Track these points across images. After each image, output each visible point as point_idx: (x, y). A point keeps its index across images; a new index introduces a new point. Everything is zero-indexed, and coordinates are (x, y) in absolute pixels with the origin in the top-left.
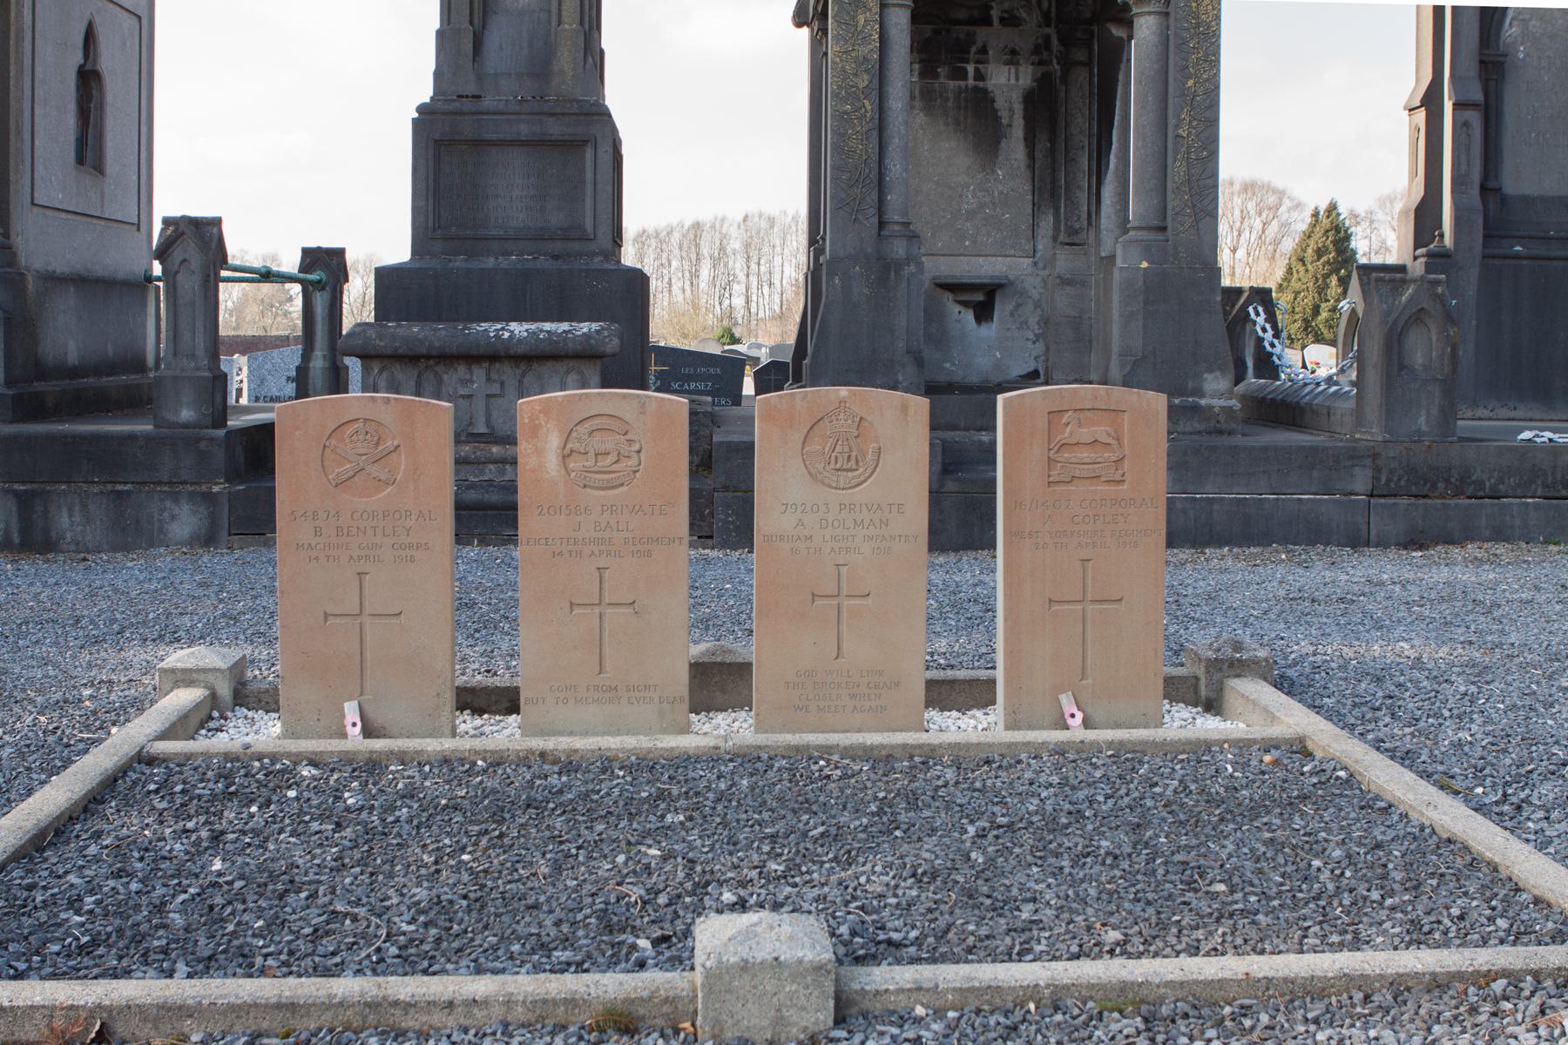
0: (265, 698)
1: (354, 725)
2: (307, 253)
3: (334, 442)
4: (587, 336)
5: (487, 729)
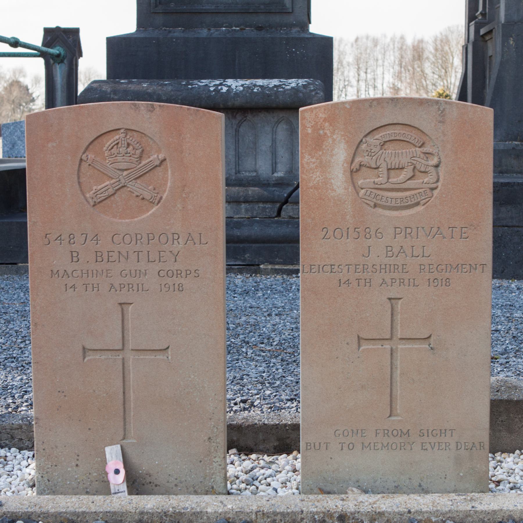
0: (18, 434)
1: (117, 472)
2: (48, 32)
3: (91, 156)
4: (295, 90)
5: (258, 472)
